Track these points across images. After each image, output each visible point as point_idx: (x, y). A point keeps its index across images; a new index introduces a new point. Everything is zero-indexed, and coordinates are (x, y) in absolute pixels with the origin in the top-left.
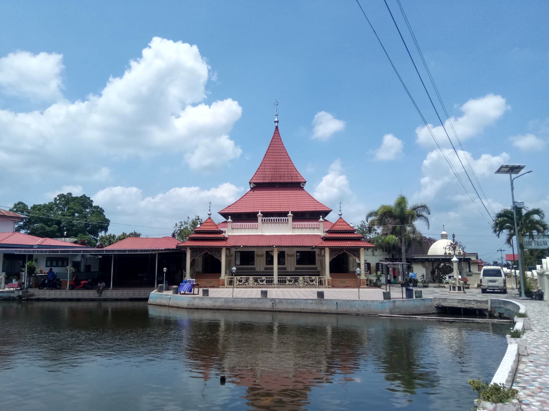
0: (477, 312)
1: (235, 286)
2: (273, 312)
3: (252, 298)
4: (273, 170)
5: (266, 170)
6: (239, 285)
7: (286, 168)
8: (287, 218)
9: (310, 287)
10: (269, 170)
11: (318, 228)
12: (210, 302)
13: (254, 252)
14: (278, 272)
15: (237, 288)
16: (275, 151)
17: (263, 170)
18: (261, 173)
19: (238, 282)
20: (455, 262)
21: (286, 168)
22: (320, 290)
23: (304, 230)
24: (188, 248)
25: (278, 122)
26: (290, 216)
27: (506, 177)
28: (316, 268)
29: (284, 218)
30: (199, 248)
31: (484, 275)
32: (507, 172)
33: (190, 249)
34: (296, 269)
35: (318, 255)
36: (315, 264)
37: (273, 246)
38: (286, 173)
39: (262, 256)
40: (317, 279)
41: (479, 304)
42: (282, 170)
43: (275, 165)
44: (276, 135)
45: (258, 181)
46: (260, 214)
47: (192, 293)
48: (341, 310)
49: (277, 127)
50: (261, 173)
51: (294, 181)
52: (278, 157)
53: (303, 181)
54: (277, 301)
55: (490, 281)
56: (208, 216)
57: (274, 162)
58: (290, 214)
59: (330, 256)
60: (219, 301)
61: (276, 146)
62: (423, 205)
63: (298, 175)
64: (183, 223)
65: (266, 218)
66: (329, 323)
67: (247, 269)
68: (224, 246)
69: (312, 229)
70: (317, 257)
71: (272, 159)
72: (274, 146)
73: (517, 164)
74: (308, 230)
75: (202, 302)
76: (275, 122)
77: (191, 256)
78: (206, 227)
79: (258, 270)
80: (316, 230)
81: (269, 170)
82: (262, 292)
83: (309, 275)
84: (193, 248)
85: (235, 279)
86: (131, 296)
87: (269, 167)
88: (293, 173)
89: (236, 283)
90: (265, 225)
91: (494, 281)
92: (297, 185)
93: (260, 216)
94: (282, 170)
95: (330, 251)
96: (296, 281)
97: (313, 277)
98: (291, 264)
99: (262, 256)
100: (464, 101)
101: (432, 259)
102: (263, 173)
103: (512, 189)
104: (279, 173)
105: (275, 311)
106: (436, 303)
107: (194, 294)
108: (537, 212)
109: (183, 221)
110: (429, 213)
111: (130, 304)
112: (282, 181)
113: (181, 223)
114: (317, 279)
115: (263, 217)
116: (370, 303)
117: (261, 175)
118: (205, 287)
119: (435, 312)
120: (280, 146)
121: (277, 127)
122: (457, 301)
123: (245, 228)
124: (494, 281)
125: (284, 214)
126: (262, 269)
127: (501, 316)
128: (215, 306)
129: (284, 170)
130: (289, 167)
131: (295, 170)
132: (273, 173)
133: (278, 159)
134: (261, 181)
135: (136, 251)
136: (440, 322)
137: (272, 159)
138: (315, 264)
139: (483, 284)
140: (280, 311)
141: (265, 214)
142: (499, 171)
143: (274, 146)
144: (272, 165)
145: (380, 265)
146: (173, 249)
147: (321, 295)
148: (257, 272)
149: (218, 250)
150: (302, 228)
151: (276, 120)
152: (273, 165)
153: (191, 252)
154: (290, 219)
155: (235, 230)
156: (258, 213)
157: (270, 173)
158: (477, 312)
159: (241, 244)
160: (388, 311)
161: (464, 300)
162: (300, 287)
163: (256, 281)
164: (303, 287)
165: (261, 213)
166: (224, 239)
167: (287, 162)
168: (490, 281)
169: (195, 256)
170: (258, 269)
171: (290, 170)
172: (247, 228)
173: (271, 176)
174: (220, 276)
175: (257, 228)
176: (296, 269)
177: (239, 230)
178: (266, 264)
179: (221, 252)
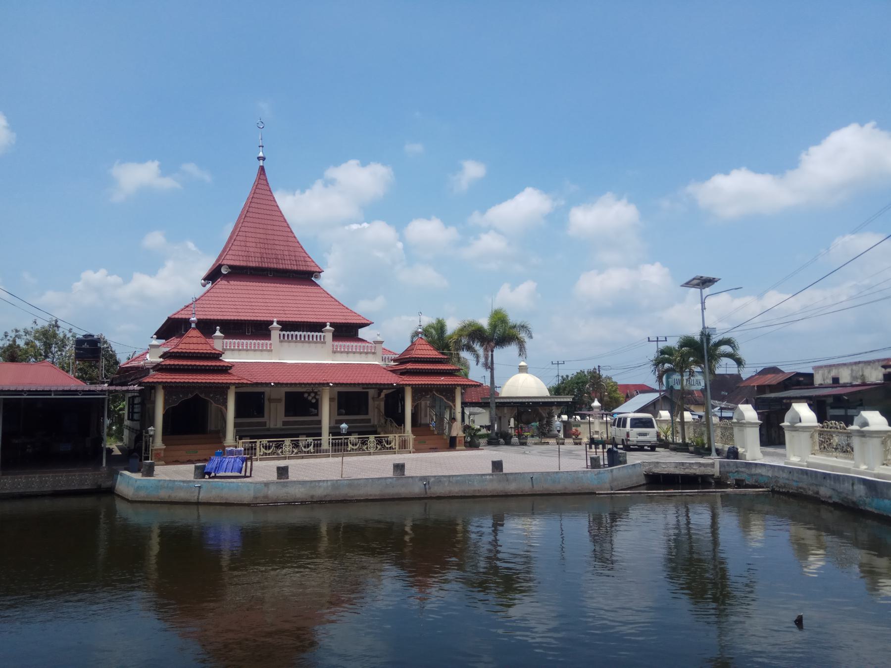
0: (700, 480)
1: (258, 456)
2: (424, 499)
3: (386, 478)
5: (248, 244)
6: (266, 454)
7: (285, 243)
8: (322, 334)
9: (385, 453)
11: (374, 353)
12: (302, 490)
13: (263, 393)
15: (261, 460)
16: (262, 211)
17: (243, 243)
18: (239, 248)
19: (263, 450)
20: (597, 407)
21: (285, 243)
22: (282, 463)
23: (351, 355)
24: (161, 386)
25: (264, 159)
26: (328, 331)
27: (694, 292)
28: (369, 421)
29: (319, 334)
30: (184, 387)
31: (632, 426)
32: (694, 286)
33: (164, 388)
34: (285, 423)
35: (373, 398)
36: (367, 413)
37: (328, 384)
38: (286, 253)
39: (279, 400)
40: (397, 438)
41: (702, 468)
43: (264, 236)
44: (261, 181)
45: (237, 263)
46: (275, 324)
47: (243, 474)
48: (539, 488)
49: (262, 169)
50: (239, 248)
51: (301, 268)
52: (269, 222)
53: (318, 270)
54: (432, 479)
55: (640, 434)
57: (261, 231)
58: (328, 327)
60: (320, 487)
61: (260, 206)
63: (308, 259)
64: (22, 333)
65: (286, 333)
66: (324, 519)
67: (250, 424)
68: (409, 385)
69: (363, 355)
70: (370, 401)
73: (711, 275)
74: (358, 355)
75: (284, 490)
76: (259, 158)
77: (413, 400)
78: (192, 346)
79: (272, 426)
80: (370, 356)
81: (254, 245)
82: (279, 469)
84: (171, 387)
85: (258, 444)
86: (48, 488)
87: (253, 240)
88: (297, 254)
89: (260, 451)
90: (286, 344)
91: (645, 434)
92: (305, 276)
93: (275, 328)
94: (278, 247)
96: (364, 443)
98: (275, 416)
99: (279, 400)
100: (338, 160)
101: (528, 403)
102: (244, 248)
103: (703, 309)
104: (273, 252)
105: (431, 498)
106: (644, 470)
107: (245, 477)
108: (728, 342)
109: (21, 328)
111: (47, 505)
112: (281, 267)
113: (17, 331)
114: (397, 438)
115: (281, 330)
116: (581, 475)
117: (240, 253)
118: (199, 461)
119: (116, 498)
120: (270, 203)
121: (262, 169)
122: (673, 465)
123: (247, 350)
124: (645, 434)
125: (318, 327)
126: (279, 425)
127: (739, 484)
128: (312, 497)
129: (282, 248)
130: (291, 244)
131: (300, 250)
132: (263, 251)
133: (269, 227)
135: (49, 392)
136: (651, 498)
138: (263, 416)
139: (631, 439)
140: (439, 498)
141: (287, 326)
142: (688, 284)
144: (259, 235)
147: (399, 468)
148: (269, 430)
149: (223, 389)
150: (348, 353)
151: (261, 154)
153: (165, 395)
154: (329, 336)
155: (338, 355)
156: (272, 322)
157: (256, 250)
158: (700, 480)
159: (248, 378)
160: (608, 485)
161: (683, 464)
162: (370, 454)
163: (296, 445)
164: (374, 454)
165: (279, 323)
166: (225, 370)
167: (285, 234)
168: (640, 434)
169: (420, 399)
170: (272, 425)
171: (291, 249)
172: (251, 350)
173: (259, 255)
175: (271, 351)
176: (285, 423)
177: (236, 353)
179: (227, 395)
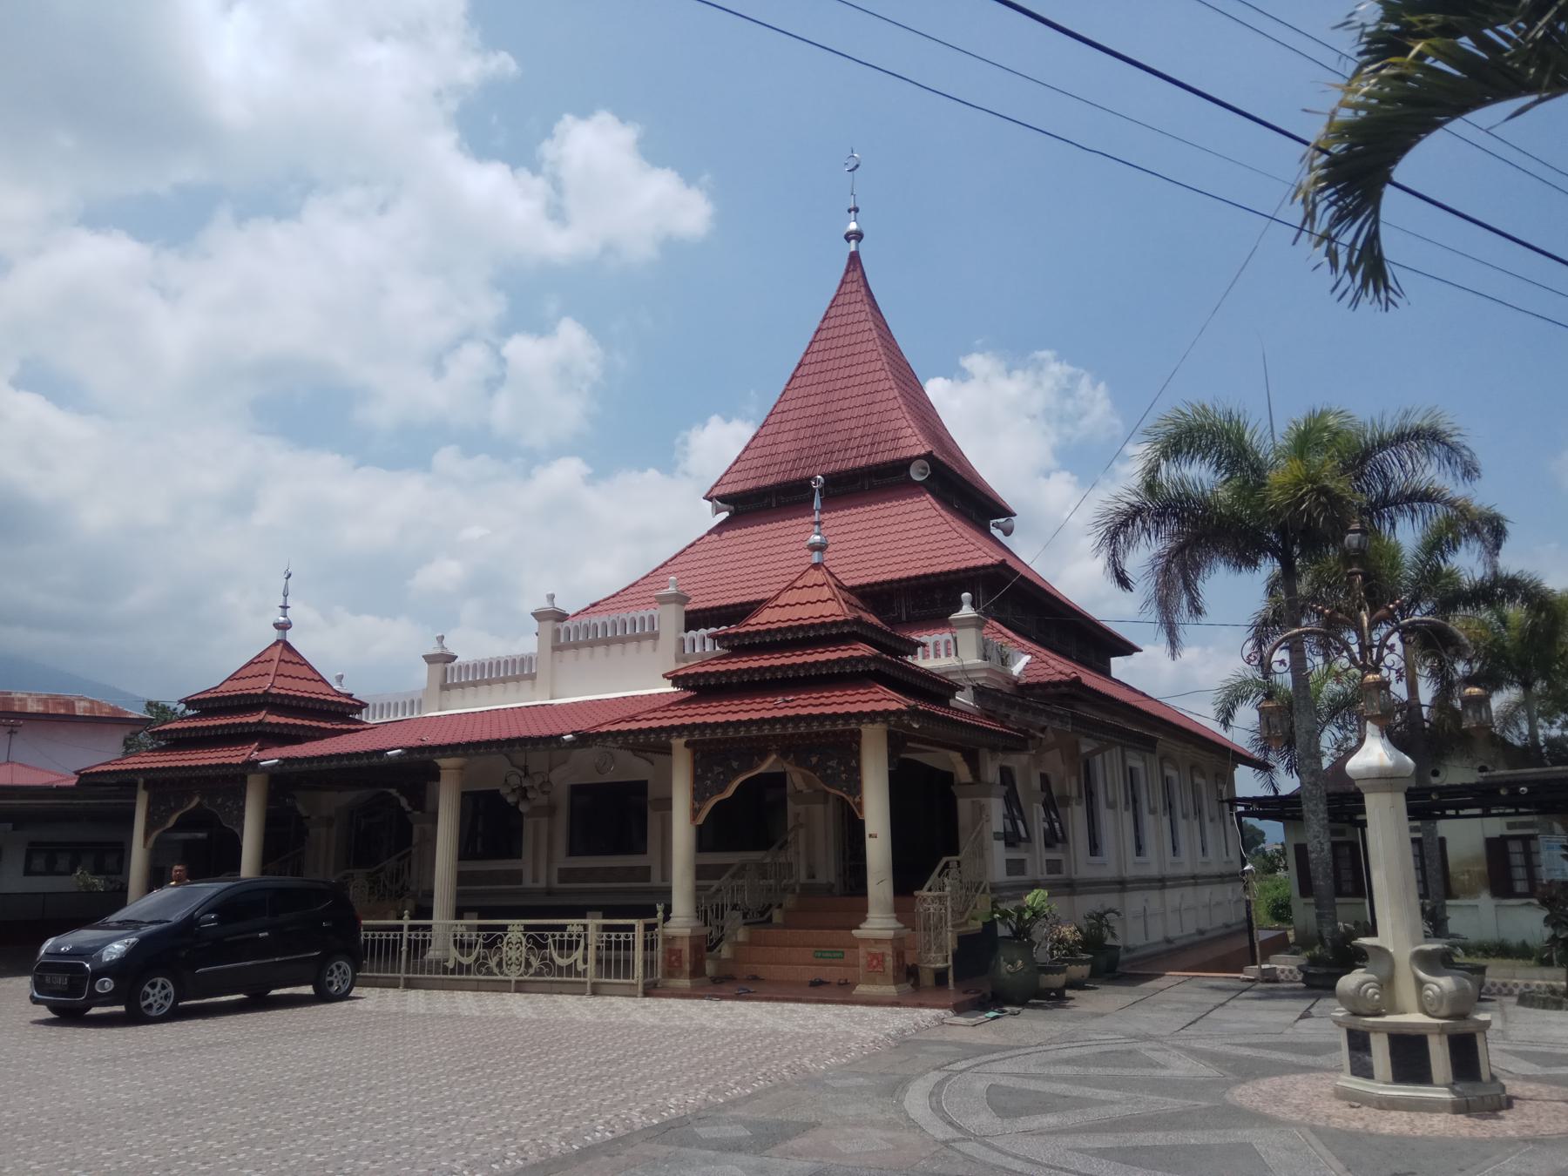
4: (809, 432)
10: (791, 435)
14: (460, 895)
20: (1384, 779)
25: (858, 236)
34: (566, 875)
42: (839, 426)
45: (739, 487)
49: (854, 258)
56: (274, 635)
59: (698, 795)
62: (1416, 421)
67: (610, 874)
71: (813, 390)
72: (830, 334)
76: (848, 237)
83: (609, 912)
94: (839, 426)
95: (696, 764)
97: (574, 925)
110: (1470, 471)
121: (854, 258)
134: (750, 485)
137: (813, 390)
143: (830, 334)
145: (1515, 847)
146: (59, 792)
151: (853, 226)
152: (815, 410)
155: (455, 694)
164: (520, 987)
174: (861, 913)
178: (572, 852)
